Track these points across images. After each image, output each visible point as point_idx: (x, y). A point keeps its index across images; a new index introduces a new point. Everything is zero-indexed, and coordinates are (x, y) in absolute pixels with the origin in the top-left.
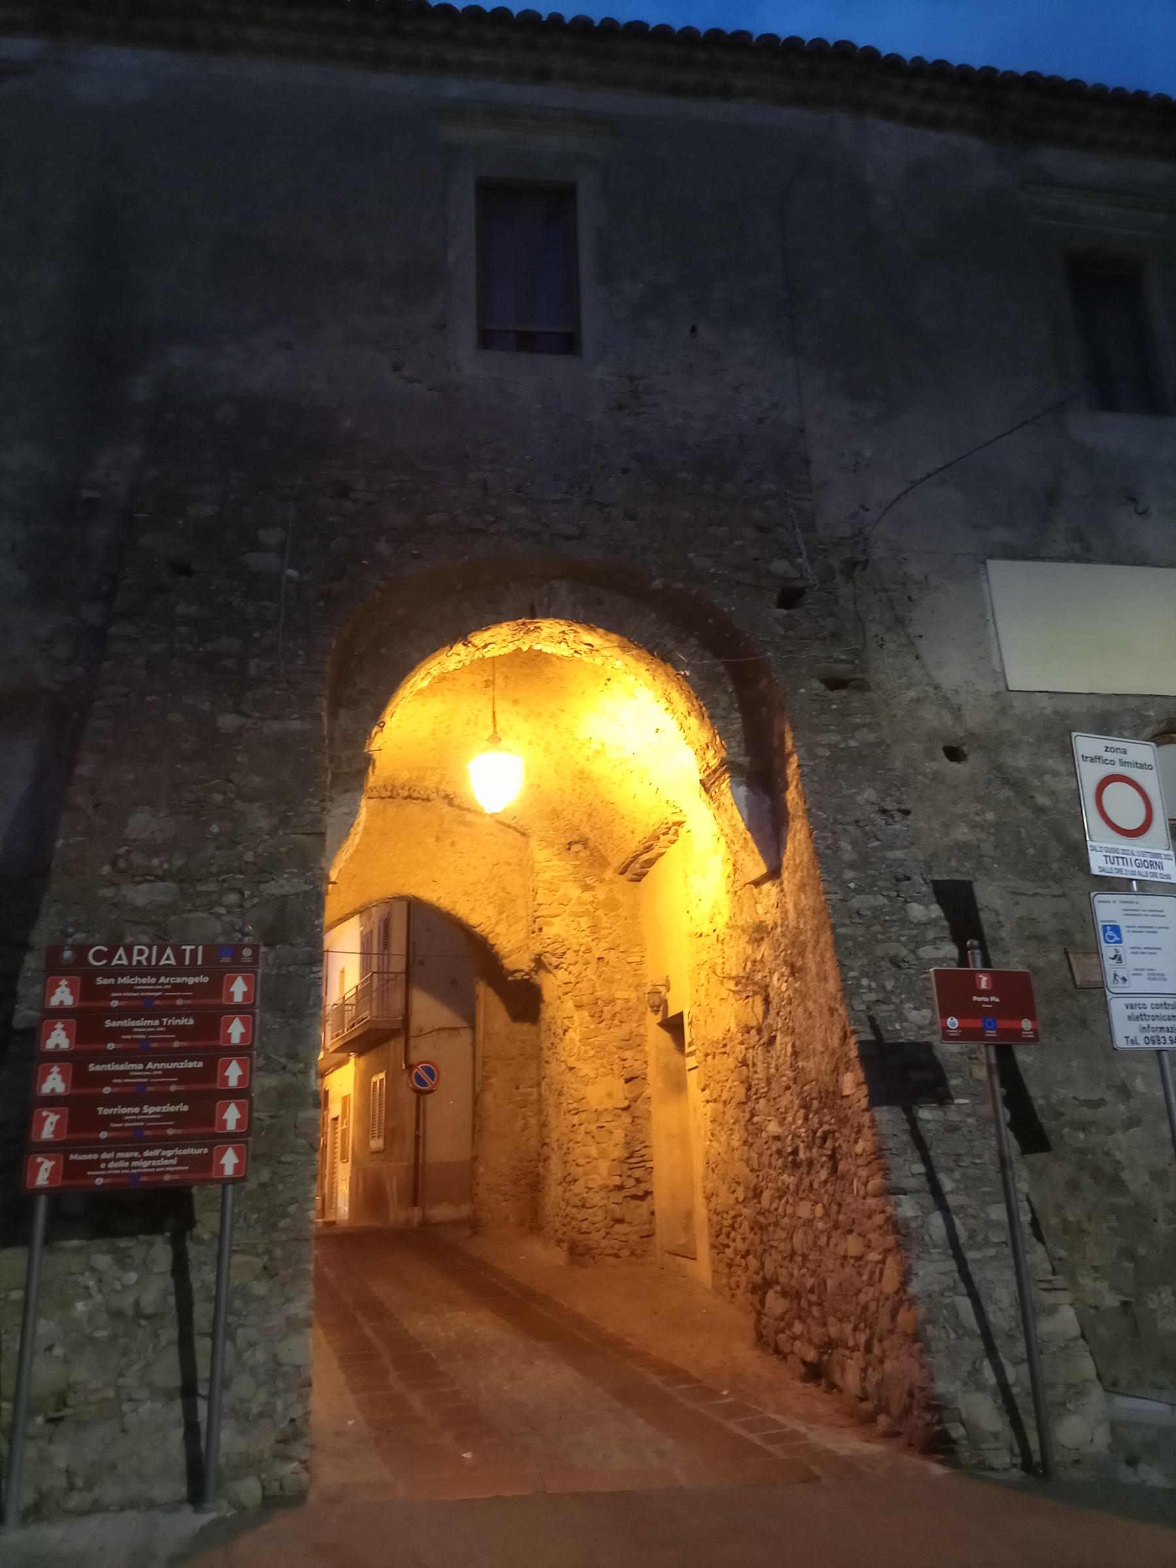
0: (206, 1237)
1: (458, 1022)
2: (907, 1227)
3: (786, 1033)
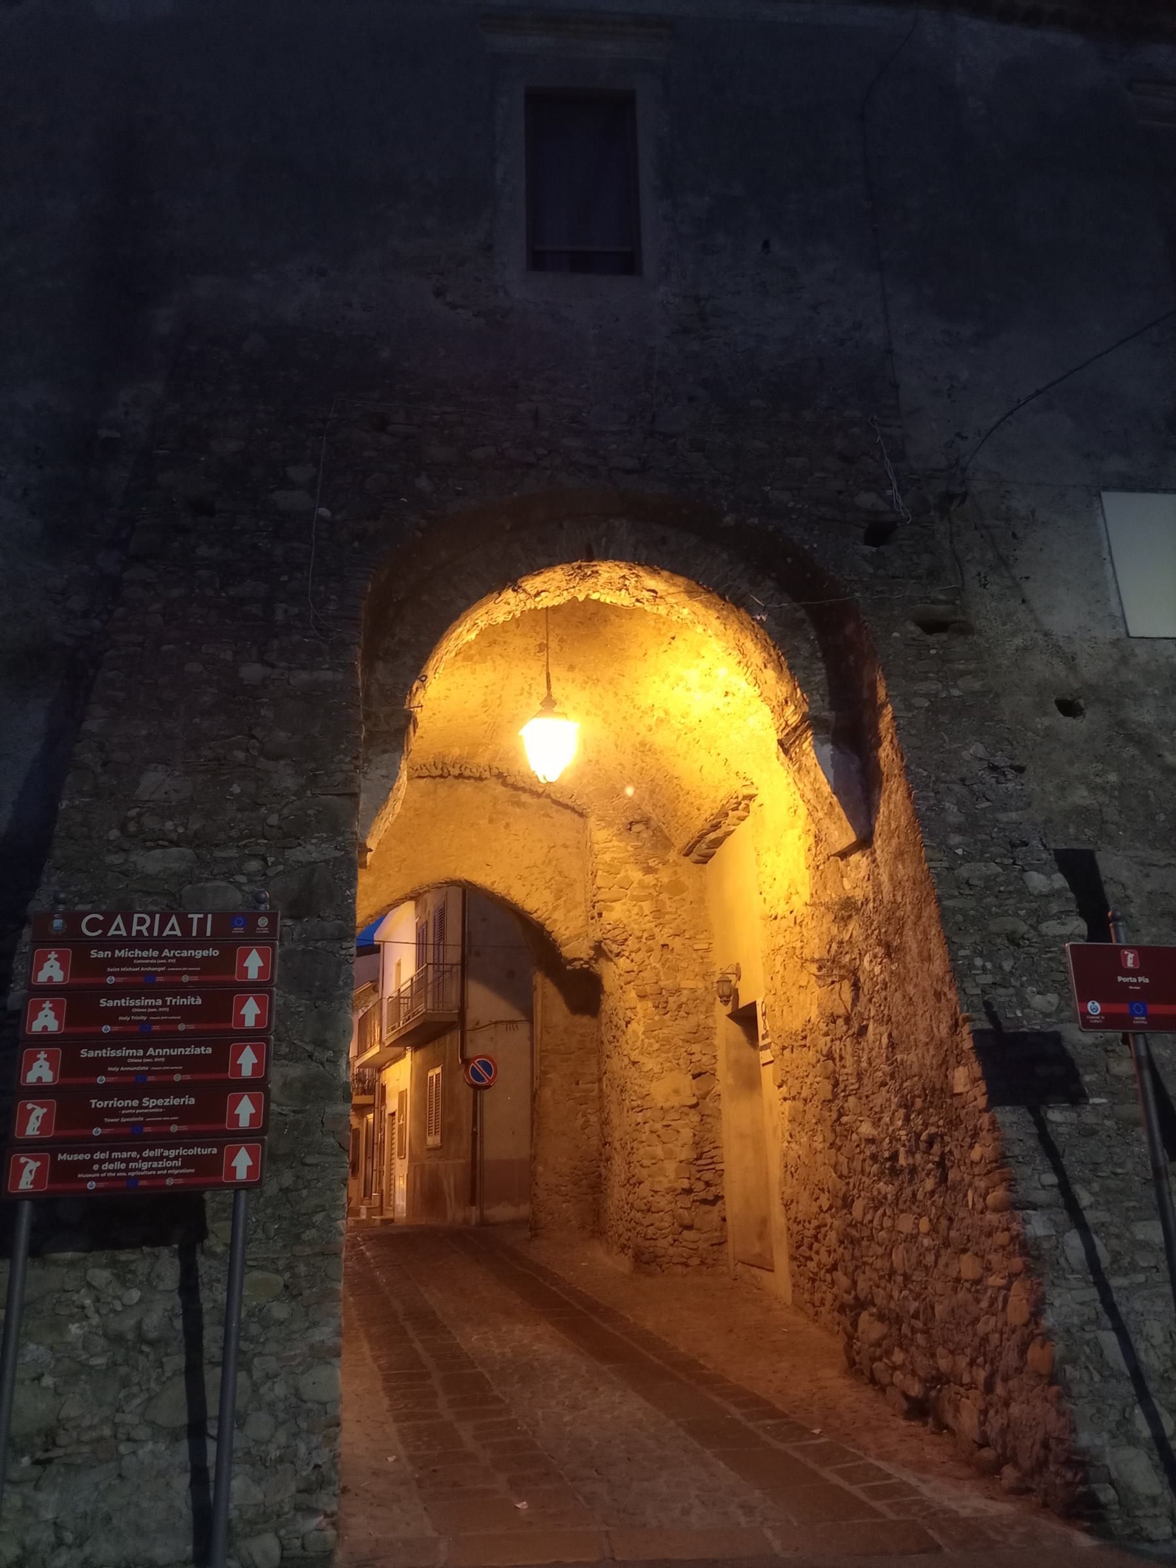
0: (220, 1249)
1: (516, 1015)
2: (1038, 1248)
3: (880, 1022)
